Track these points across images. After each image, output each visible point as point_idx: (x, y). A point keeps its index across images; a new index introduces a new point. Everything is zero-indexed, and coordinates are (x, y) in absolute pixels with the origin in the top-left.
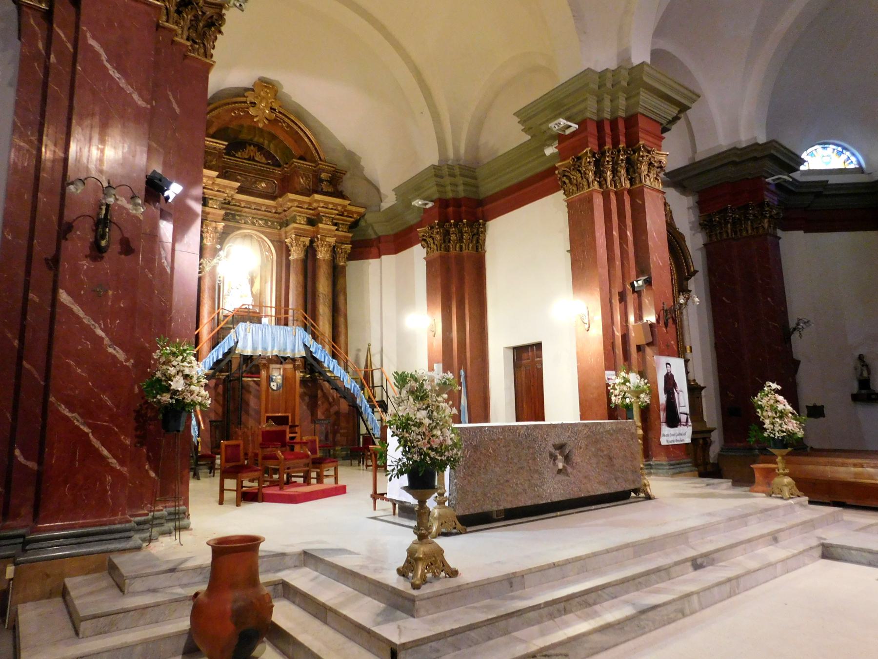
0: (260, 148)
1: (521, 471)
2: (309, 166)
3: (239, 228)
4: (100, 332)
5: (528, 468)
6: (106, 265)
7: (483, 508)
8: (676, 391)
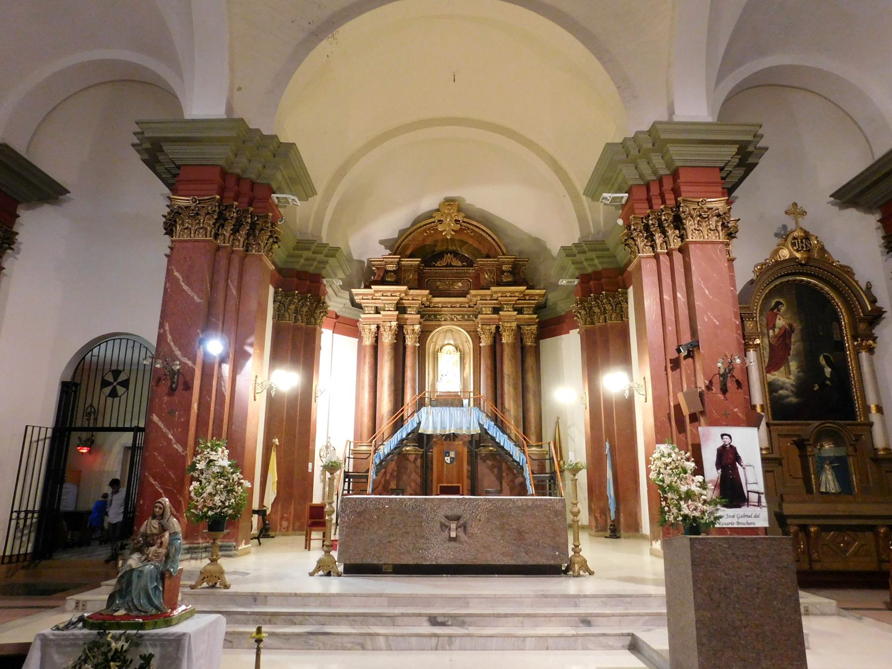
0: (456, 254)
1: (406, 535)
2: (493, 261)
3: (439, 326)
4: (171, 436)
5: (414, 534)
6: (176, 398)
7: (364, 560)
8: (741, 466)
